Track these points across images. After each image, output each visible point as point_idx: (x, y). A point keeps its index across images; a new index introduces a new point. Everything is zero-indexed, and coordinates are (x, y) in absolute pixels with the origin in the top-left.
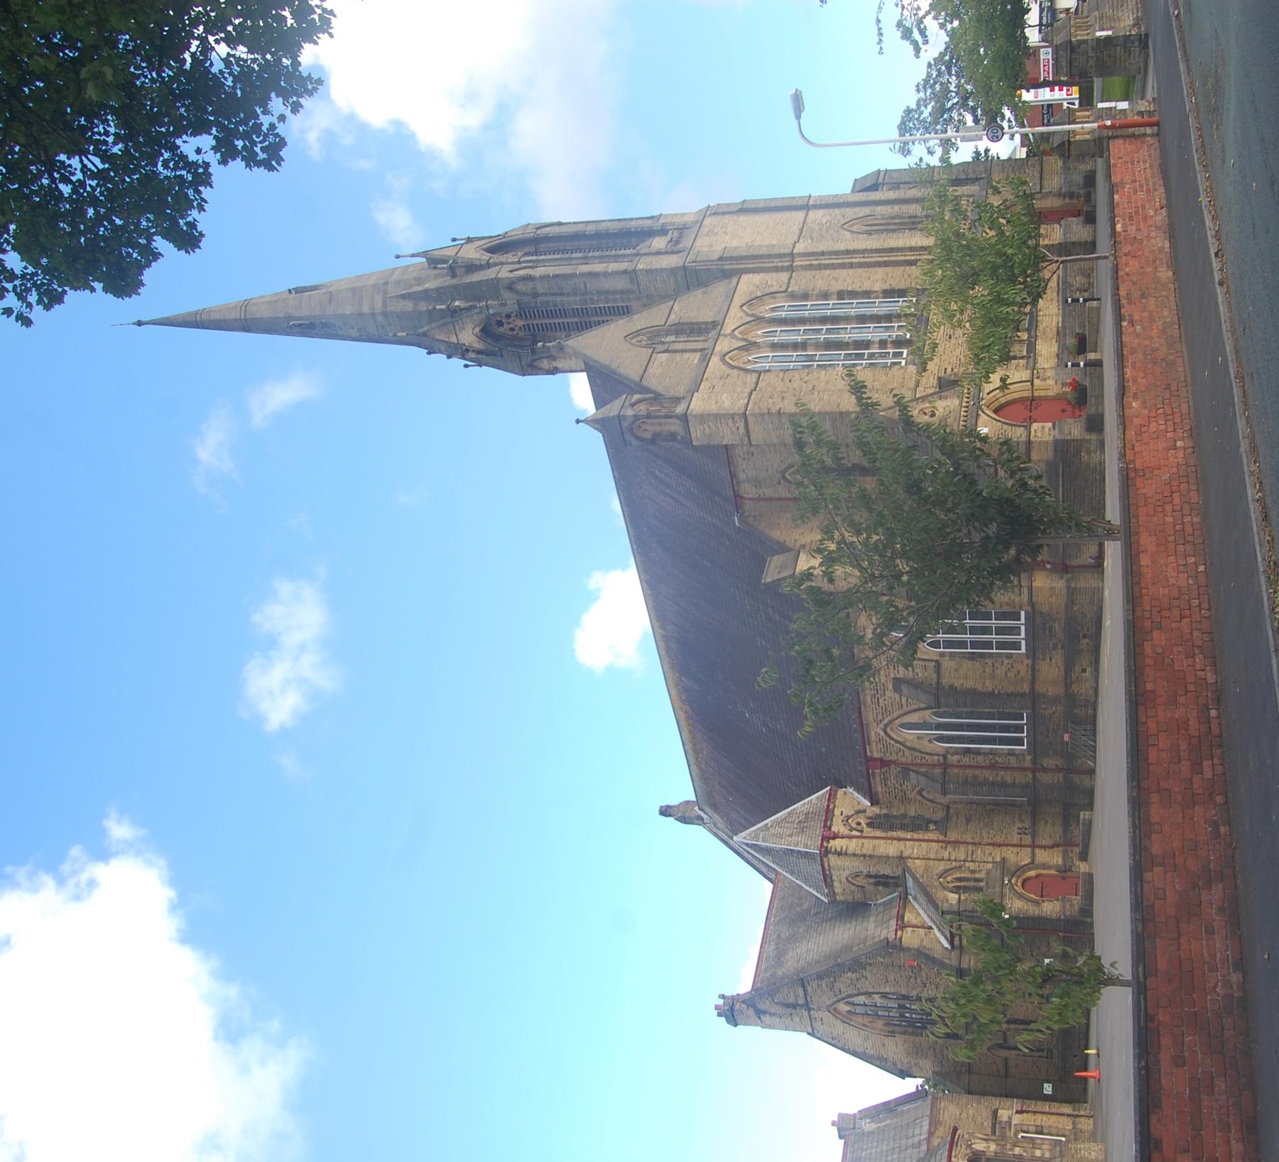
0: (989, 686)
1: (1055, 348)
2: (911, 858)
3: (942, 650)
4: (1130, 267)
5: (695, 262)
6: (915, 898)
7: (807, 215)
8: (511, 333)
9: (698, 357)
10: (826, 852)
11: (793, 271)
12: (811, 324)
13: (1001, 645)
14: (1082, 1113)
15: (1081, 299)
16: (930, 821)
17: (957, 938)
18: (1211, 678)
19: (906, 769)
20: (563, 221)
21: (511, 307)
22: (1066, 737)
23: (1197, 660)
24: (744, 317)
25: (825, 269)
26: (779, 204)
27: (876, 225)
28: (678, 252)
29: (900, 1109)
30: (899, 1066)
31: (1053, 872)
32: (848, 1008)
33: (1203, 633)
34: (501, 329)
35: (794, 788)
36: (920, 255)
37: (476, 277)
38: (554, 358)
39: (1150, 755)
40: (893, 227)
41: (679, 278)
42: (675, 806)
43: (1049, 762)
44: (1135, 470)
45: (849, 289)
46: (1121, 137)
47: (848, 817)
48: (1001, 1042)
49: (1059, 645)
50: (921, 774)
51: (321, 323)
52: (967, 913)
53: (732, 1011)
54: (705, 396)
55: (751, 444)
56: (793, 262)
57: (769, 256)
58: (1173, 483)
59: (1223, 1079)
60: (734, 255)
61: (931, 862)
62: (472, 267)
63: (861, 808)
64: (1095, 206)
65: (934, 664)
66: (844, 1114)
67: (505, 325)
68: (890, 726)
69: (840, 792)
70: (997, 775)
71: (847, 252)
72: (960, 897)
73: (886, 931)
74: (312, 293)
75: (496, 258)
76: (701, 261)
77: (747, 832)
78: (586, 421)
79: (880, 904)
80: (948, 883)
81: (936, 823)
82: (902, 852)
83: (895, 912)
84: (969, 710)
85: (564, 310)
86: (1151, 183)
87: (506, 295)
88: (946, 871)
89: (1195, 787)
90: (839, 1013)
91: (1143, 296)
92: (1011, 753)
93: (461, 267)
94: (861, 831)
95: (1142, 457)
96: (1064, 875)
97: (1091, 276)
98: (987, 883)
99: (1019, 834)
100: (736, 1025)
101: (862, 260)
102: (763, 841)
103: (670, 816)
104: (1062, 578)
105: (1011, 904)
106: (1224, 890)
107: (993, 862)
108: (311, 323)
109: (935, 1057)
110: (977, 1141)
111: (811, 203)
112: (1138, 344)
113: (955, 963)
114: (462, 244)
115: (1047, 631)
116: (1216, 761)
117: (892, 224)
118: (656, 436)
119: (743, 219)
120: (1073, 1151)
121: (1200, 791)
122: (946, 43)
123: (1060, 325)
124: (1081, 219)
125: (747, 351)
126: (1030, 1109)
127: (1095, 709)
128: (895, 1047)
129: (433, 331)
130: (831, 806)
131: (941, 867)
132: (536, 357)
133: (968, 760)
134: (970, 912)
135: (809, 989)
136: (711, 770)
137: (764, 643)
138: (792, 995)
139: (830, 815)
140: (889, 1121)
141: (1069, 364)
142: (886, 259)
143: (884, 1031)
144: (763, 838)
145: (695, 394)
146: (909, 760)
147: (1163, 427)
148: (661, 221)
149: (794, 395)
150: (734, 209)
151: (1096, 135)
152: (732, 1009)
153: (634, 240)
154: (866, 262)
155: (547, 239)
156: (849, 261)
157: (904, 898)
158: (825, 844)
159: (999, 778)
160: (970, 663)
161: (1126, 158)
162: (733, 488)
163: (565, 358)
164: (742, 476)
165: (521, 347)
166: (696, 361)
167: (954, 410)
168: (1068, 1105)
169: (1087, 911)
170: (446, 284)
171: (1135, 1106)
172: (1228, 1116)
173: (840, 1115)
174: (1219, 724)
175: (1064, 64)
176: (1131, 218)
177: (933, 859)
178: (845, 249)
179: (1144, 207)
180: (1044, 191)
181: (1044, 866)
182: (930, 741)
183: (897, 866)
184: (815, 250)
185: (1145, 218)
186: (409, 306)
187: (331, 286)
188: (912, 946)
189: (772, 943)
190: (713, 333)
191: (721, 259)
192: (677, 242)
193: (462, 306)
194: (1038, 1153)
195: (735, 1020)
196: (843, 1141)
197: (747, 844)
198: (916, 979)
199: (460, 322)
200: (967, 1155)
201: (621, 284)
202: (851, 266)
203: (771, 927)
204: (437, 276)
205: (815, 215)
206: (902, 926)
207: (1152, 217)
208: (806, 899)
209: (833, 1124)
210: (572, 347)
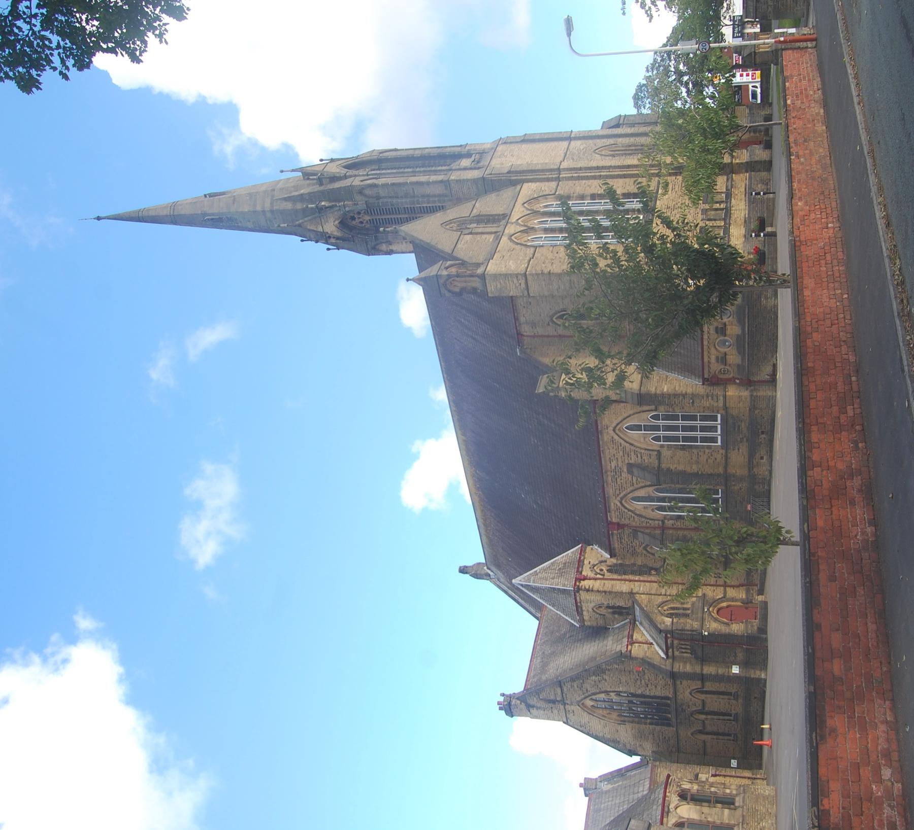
0: (695, 468)
1: (743, 231)
2: (638, 593)
3: (662, 443)
4: (796, 125)
5: (491, 174)
6: (641, 624)
7: (570, 143)
8: (359, 225)
10: (578, 589)
11: (560, 181)
13: (704, 439)
14: (758, 776)
15: (762, 193)
16: (652, 569)
17: (670, 650)
18: (852, 358)
19: (635, 531)
20: (399, 148)
21: (361, 206)
23: (843, 349)
24: (525, 211)
25: (582, 179)
26: (550, 136)
27: (619, 151)
28: (479, 168)
29: (629, 774)
30: (628, 747)
31: (739, 604)
32: (592, 703)
33: (847, 333)
34: (354, 222)
35: (556, 548)
37: (337, 185)
38: (390, 243)
39: (811, 404)
40: (630, 152)
41: (479, 186)
42: (470, 567)
44: (800, 241)
45: (599, 193)
46: (791, 49)
47: (594, 566)
48: (701, 728)
49: (745, 439)
50: (646, 534)
51: (227, 218)
52: (677, 631)
53: (510, 706)
54: (498, 262)
55: (529, 296)
56: (560, 174)
57: (543, 171)
58: (826, 248)
59: (862, 588)
60: (518, 170)
61: (653, 596)
62: (334, 179)
63: (603, 559)
64: (772, 137)
66: (589, 778)
67: (357, 219)
69: (589, 548)
71: (598, 168)
72: (673, 620)
73: (620, 646)
74: (221, 197)
75: (351, 172)
76: (495, 174)
77: (522, 576)
78: (413, 280)
79: (616, 628)
80: (665, 611)
81: (656, 570)
82: (632, 589)
83: (626, 633)
84: (681, 486)
85: (398, 208)
86: (811, 76)
87: (358, 198)
88: (664, 602)
89: (842, 421)
90: (586, 707)
91: (805, 141)
93: (327, 178)
94: (604, 575)
95: (805, 234)
96: (747, 606)
97: (769, 184)
98: (692, 611)
99: (715, 577)
100: (512, 716)
101: (608, 173)
102: (534, 583)
103: (466, 573)
104: (747, 389)
106: (862, 480)
107: (696, 597)
108: (220, 218)
109: (654, 740)
110: (684, 783)
111: (572, 136)
112: (802, 169)
113: (669, 668)
114: (328, 163)
115: (736, 430)
116: (856, 406)
117: (629, 150)
118: (463, 290)
119: (524, 146)
120: (752, 790)
121: (845, 424)
122: (667, 38)
123: (747, 216)
124: (762, 146)
125: (527, 233)
126: (721, 774)
127: (769, 485)
128: (625, 733)
129: (306, 223)
130: (582, 558)
131: (660, 599)
132: (378, 242)
133: (679, 524)
134: (680, 630)
135: (565, 689)
136: (496, 538)
137: (536, 441)
138: (553, 693)
139: (581, 564)
140: (621, 783)
142: (625, 172)
143: (615, 720)
144: (534, 580)
145: (491, 261)
146: (638, 524)
147: (819, 216)
148: (467, 148)
149: (560, 262)
150: (519, 140)
151: (774, 48)
152: (509, 704)
153: (448, 161)
154: (611, 175)
155: (387, 160)
156: (599, 174)
157: (633, 623)
158: (578, 584)
160: (682, 452)
161: (794, 62)
162: (516, 328)
163: (398, 243)
164: (522, 319)
165: (367, 235)
166: (491, 240)
168: (748, 771)
169: (763, 630)
170: (316, 190)
171: (802, 592)
172: (866, 609)
173: (585, 779)
174: (858, 384)
175: (751, 10)
176: (797, 96)
177: (654, 595)
178: (596, 166)
179: (806, 89)
181: (733, 600)
182: (653, 510)
183: (629, 600)
184: (575, 166)
185: (807, 96)
186: (289, 206)
187: (234, 192)
188: (638, 656)
189: (539, 658)
190: (503, 222)
191: (509, 172)
192: (478, 162)
193: (327, 205)
194: (728, 791)
195: (512, 712)
196: (587, 798)
197: (522, 585)
198: (641, 681)
199: (325, 217)
200: (678, 791)
201: (439, 190)
203: (538, 647)
204: (309, 185)
206: (631, 642)
207: (811, 95)
208: (563, 627)
209: (581, 785)
210: (404, 231)
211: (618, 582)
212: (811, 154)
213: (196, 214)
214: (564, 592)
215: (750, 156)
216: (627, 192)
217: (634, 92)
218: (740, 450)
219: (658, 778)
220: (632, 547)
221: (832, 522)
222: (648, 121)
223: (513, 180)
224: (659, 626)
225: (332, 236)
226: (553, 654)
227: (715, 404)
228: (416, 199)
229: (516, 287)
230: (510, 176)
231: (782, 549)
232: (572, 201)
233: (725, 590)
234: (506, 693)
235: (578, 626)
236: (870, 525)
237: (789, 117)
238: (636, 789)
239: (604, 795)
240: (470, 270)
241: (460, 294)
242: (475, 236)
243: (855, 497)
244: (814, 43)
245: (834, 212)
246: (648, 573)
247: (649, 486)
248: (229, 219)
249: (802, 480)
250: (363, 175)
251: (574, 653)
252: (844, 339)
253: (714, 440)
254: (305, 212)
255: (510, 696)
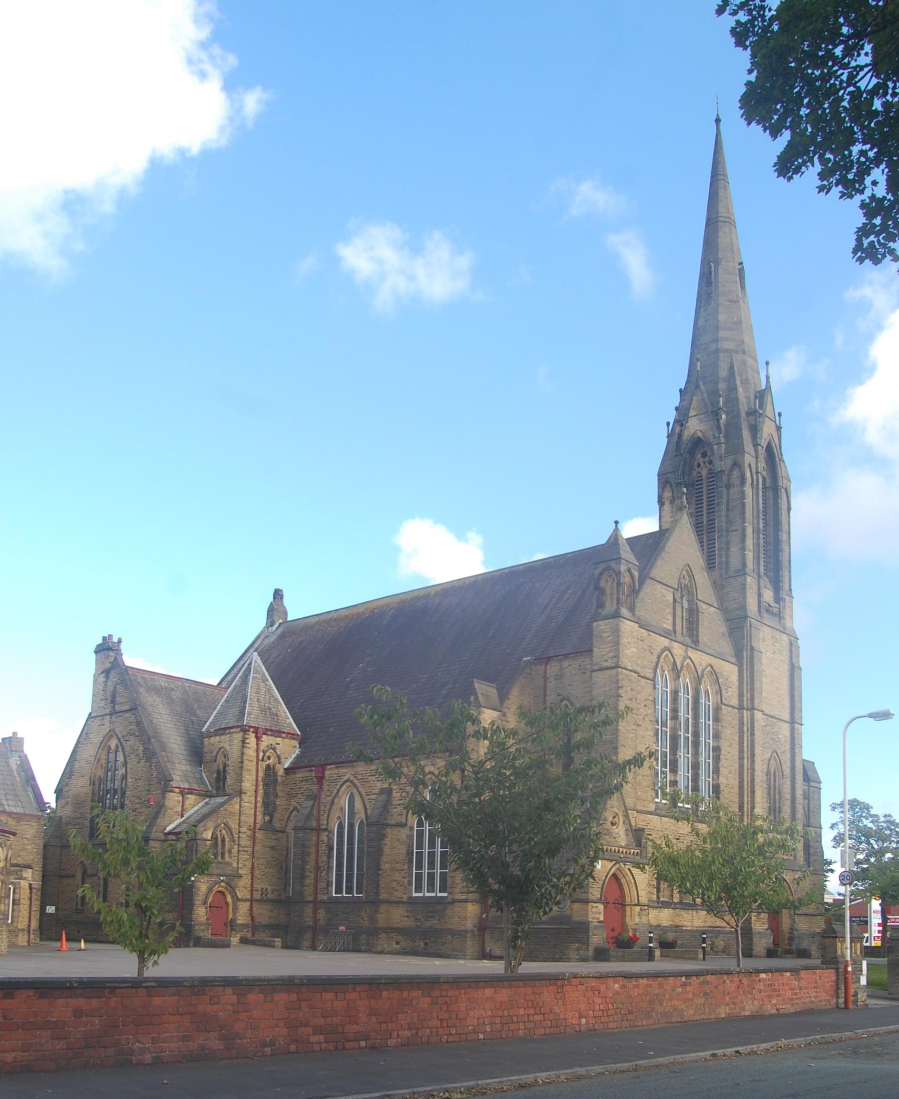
0: (386, 866)
1: (665, 923)
2: (241, 800)
4: (730, 984)
5: (751, 626)
6: (207, 804)
7: (787, 722)
8: (695, 464)
9: (669, 628)
10: (245, 730)
11: (739, 709)
12: (693, 724)
13: (419, 877)
14: (32, 936)
15: (705, 945)
16: (272, 817)
17: (174, 837)
18: (392, 1042)
21: (719, 465)
22: (342, 928)
23: (406, 1032)
24: (701, 668)
25: (739, 736)
26: (796, 699)
28: (760, 612)
29: (30, 789)
30: (66, 789)
31: (231, 916)
32: (113, 746)
34: (699, 456)
36: (748, 815)
37: (746, 434)
43: (322, 914)
44: (563, 986)
45: (722, 756)
46: (838, 979)
47: (274, 749)
48: (88, 872)
51: (711, 293)
52: (195, 845)
56: (747, 710)
57: (752, 690)
59: (65, 1047)
61: (238, 818)
62: (755, 430)
63: (283, 760)
64: (781, 957)
65: (404, 822)
66: (23, 742)
67: (703, 459)
68: (351, 785)
69: (296, 743)
70: (311, 872)
71: (753, 755)
73: (179, 779)
74: (739, 284)
75: (762, 451)
77: (261, 664)
78: (616, 530)
79: (201, 775)
80: (220, 831)
81: (270, 821)
82: (246, 793)
83: (195, 787)
84: (365, 850)
86: (798, 1001)
87: (729, 461)
90: (109, 740)
91: (706, 994)
92: (329, 884)
93: (756, 421)
94: (263, 760)
99: (262, 889)
100: (96, 652)
101: (745, 767)
102: (254, 678)
103: (274, 598)
104: (474, 926)
105: (203, 882)
107: (238, 868)
108: (711, 283)
110: (5, 851)
111: (796, 725)
113: (153, 835)
114: (775, 422)
115: (430, 914)
116: (324, 1045)
118: (602, 591)
119: (786, 667)
124: (771, 946)
126: (33, 895)
127: (365, 951)
128: (81, 785)
129: (700, 394)
130: (283, 735)
131: (234, 826)
132: (674, 486)
134: (196, 848)
135: (128, 715)
137: (422, 680)
141: (652, 935)
142: (746, 788)
143: (95, 774)
144: (256, 678)
145: (637, 625)
146: (323, 800)
147: (597, 1008)
148: (787, 598)
150: (794, 661)
151: (840, 959)
152: (110, 649)
153: (771, 574)
154: (743, 770)
155: (776, 497)
156: (746, 757)
157: (206, 794)
158: (251, 730)
159: (308, 874)
160: (404, 851)
163: (672, 512)
164: (566, 664)
165: (683, 473)
166: (665, 626)
167: (616, 841)
169: (199, 943)
170: (741, 407)
172: (34, 1051)
176: (770, 985)
177: (240, 819)
180: (796, 917)
181: (235, 909)
182: (339, 818)
184: (756, 728)
185: (770, 997)
186: (723, 373)
187: (744, 302)
189: (166, 684)
190: (688, 641)
191: (752, 648)
192: (768, 611)
197: (250, 664)
198: (139, 804)
201: (735, 563)
202: (741, 758)
203: (180, 683)
204: (748, 398)
205: (785, 729)
206: (183, 792)
207: (770, 1002)
209: (15, 734)
210: (681, 518)
211: (254, 777)
212: (686, 1000)
213: (718, 252)
214: (242, 714)
215: (759, 933)
216: (721, 789)
217: (861, 800)
218: (406, 919)
219: (25, 823)
220: (297, 794)
221: (158, 1015)
222: (811, 815)
223: (743, 653)
224: (201, 824)
225: (683, 428)
226: (171, 701)
227: (457, 890)
228: (724, 533)
229: (603, 656)
230: (747, 651)
231: (134, 957)
232: (713, 725)
233: (246, 900)
234: (122, 644)
235: (203, 730)
236: (154, 1058)
237: (741, 975)
238: (12, 797)
239: (4, 760)
240: (626, 600)
241: (597, 588)
242: (671, 606)
243: (194, 1042)
244: (843, 1006)
245: (602, 1025)
246: (266, 812)
247: (366, 814)
248: (709, 295)
249: (218, 981)
250: (757, 468)
251: (172, 726)
252: (420, 1034)
253: (419, 888)
254: (715, 393)
255: (119, 650)
